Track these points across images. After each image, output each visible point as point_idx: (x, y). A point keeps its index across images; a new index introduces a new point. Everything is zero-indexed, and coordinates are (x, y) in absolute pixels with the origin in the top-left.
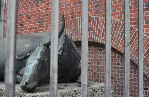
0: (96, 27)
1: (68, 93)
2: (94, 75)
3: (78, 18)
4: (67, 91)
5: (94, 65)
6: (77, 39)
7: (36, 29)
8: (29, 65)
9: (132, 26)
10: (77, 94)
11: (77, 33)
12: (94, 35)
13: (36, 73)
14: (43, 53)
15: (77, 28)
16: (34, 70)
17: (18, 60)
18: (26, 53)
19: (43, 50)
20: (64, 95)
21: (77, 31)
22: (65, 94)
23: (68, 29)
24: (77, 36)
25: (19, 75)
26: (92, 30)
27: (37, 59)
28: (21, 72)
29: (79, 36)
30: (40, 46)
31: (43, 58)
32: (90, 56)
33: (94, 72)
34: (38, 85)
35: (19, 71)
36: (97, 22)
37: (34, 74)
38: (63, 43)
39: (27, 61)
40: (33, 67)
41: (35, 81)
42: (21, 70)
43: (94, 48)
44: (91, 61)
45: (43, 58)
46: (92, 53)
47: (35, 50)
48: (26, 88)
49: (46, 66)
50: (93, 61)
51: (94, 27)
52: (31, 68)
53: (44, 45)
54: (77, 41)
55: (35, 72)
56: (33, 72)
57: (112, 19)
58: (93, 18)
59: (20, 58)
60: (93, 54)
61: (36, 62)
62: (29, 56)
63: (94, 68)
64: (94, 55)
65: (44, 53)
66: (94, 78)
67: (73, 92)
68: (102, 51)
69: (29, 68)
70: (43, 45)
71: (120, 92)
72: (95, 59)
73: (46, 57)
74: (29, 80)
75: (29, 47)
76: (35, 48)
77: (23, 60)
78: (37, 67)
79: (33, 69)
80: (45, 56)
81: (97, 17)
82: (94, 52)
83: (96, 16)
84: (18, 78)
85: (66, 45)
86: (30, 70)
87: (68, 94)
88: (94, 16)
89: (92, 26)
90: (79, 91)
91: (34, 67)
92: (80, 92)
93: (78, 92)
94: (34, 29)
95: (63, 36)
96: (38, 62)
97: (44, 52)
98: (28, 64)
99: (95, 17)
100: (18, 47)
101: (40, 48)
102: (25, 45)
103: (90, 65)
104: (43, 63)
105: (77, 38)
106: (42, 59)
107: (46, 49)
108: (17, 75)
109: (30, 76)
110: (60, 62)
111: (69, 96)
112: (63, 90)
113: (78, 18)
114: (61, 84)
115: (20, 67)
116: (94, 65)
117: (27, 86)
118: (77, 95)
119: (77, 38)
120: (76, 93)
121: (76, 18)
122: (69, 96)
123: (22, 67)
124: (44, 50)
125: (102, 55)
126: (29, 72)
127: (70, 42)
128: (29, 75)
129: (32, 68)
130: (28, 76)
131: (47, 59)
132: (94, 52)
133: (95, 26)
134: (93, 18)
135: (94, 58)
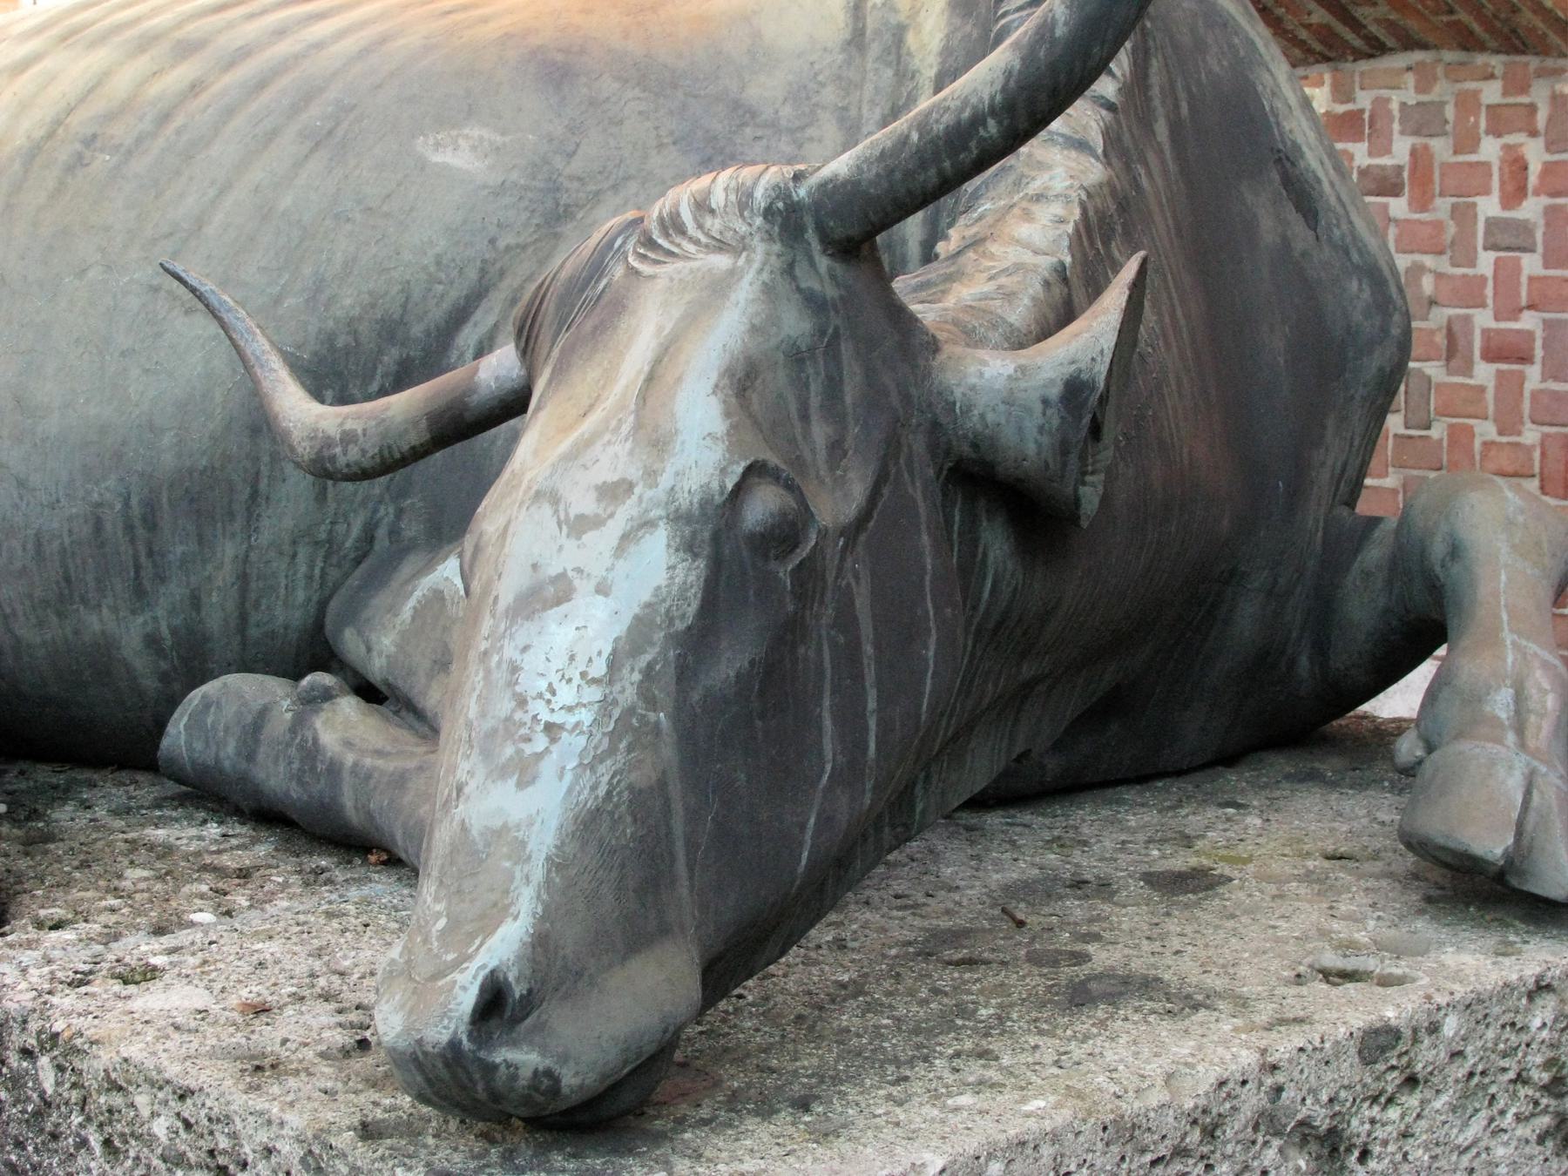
1: (1252, 1101)
8: (524, 632)
10: (1412, 1082)
13: (662, 784)
14: (778, 379)
18: (456, 294)
19: (773, 320)
20: (1180, 1152)
22: (1210, 1133)
25: (349, 706)
27: (678, 518)
28: (386, 642)
30: (720, 246)
31: (775, 475)
32: (1525, 228)
34: (705, 998)
35: (352, 614)
37: (638, 797)
40: (599, 669)
41: (664, 931)
42: (381, 600)
44: (1529, 322)
45: (775, 475)
46: (1548, 169)
47: (617, 306)
48: (496, 1097)
49: (846, 620)
52: (566, 695)
53: (793, 208)
55: (643, 777)
56: (605, 771)
59: (348, 438)
61: (661, 578)
62: (514, 404)
65: (802, 386)
67: (1349, 1069)
69: (531, 683)
70: (768, 213)
73: (836, 448)
74: (541, 943)
75: (500, 190)
76: (618, 271)
77: (418, 454)
78: (685, 674)
79: (606, 704)
80: (820, 432)
84: (334, 769)
85: (1162, 129)
86: (551, 729)
87: (1267, 1122)
90: (1451, 1025)
91: (632, 677)
92: (1457, 1055)
93: (1426, 1056)
96: (692, 574)
97: (797, 357)
98: (750, 276)
101: (719, 287)
102: (423, 145)
103: (1521, 378)
104: (784, 571)
106: (763, 506)
107: (831, 292)
108: (327, 695)
109: (556, 864)
111: (1271, 1155)
114: (1085, 817)
115: (368, 537)
117: (502, 1055)
118: (1412, 1100)
120: (1394, 1078)
122: (1271, 1155)
123: (394, 532)
124: (796, 324)
126: (525, 772)
127: (1215, 63)
128: (543, 841)
129: (594, 694)
130: (519, 852)
131: (858, 491)
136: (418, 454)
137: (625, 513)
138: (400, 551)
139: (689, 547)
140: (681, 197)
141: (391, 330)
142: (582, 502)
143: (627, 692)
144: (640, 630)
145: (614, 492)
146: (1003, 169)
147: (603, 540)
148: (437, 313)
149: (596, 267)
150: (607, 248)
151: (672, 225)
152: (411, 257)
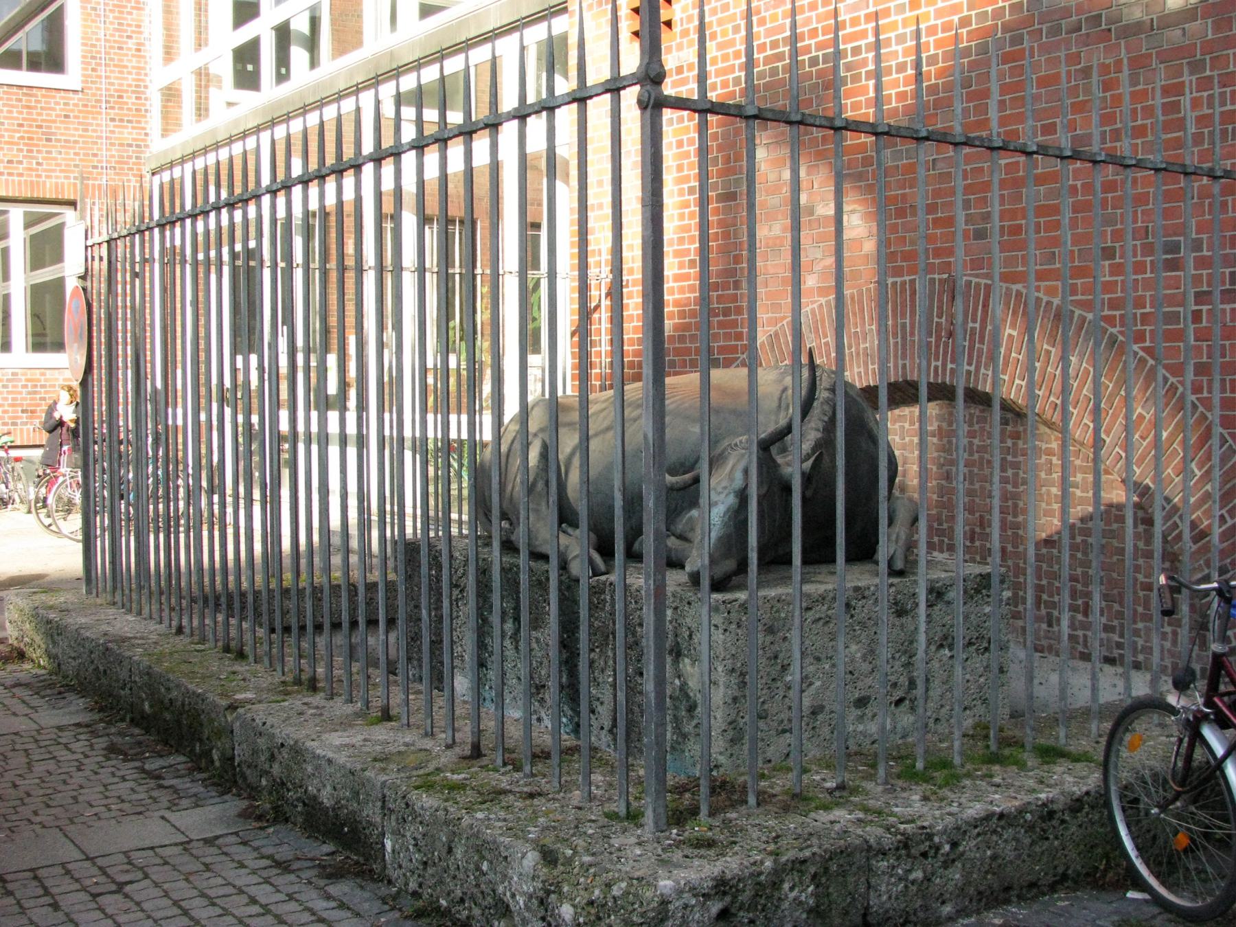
0: (977, 325)
1: (831, 595)
2: (978, 530)
3: (907, 278)
4: (830, 587)
5: (977, 486)
6: (904, 374)
7: (724, 315)
9: (1114, 330)
10: (864, 597)
11: (904, 346)
12: (979, 357)
15: (904, 326)
16: (725, 525)
17: (671, 489)
21: (904, 338)
23: (867, 327)
24: (904, 357)
25: (673, 538)
26: (973, 329)
29: (912, 358)
32: (975, 491)
33: (977, 515)
36: (984, 306)
38: (826, 419)
39: (642, 59)
43: (977, 413)
50: (976, 470)
51: (971, 325)
54: (906, 382)
57: (1041, 295)
58: (969, 283)
60: (974, 437)
63: (977, 500)
64: (976, 441)
66: (977, 543)
67: (851, 593)
68: (1009, 428)
71: (1080, 602)
72: (981, 458)
77: (690, 485)
78: (736, 517)
81: (983, 281)
82: (976, 427)
83: (977, 276)
88: (970, 275)
89: (965, 322)
90: (872, 588)
93: (866, 593)
94: (718, 315)
95: (826, 389)
96: (737, 501)
99: (974, 280)
100: (669, 433)
101: (743, 455)
105: (904, 366)
110: (809, 493)
112: (819, 586)
113: (907, 278)
116: (977, 486)
119: (904, 366)
121: (899, 280)
125: (1009, 443)
132: (976, 427)
133: (974, 321)
134: (969, 283)
135: (976, 456)
136: (690, 485)
137: (726, 492)
138: (683, 509)
139: (736, 496)
140: (737, 440)
141: (682, 465)
142: (720, 490)
143: (726, 519)
144: (728, 510)
145: (725, 488)
146: (81, 336)
147: (723, 496)
148: (692, 460)
149: (723, 452)
150: (725, 449)
151: (736, 445)
152: (935, 774)
